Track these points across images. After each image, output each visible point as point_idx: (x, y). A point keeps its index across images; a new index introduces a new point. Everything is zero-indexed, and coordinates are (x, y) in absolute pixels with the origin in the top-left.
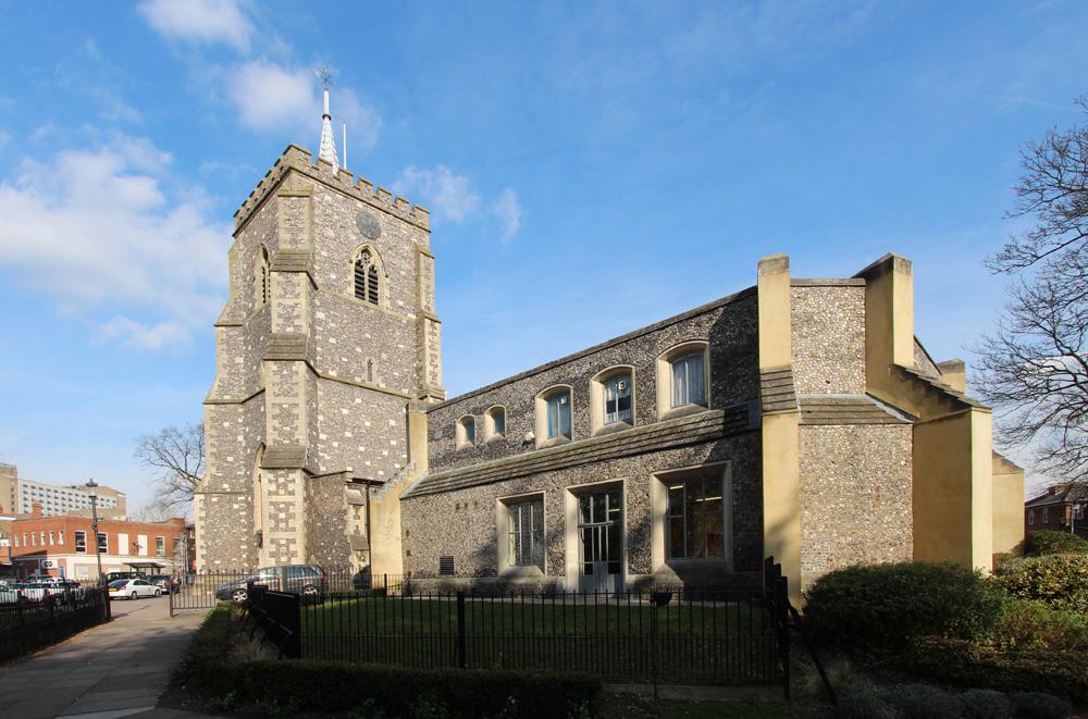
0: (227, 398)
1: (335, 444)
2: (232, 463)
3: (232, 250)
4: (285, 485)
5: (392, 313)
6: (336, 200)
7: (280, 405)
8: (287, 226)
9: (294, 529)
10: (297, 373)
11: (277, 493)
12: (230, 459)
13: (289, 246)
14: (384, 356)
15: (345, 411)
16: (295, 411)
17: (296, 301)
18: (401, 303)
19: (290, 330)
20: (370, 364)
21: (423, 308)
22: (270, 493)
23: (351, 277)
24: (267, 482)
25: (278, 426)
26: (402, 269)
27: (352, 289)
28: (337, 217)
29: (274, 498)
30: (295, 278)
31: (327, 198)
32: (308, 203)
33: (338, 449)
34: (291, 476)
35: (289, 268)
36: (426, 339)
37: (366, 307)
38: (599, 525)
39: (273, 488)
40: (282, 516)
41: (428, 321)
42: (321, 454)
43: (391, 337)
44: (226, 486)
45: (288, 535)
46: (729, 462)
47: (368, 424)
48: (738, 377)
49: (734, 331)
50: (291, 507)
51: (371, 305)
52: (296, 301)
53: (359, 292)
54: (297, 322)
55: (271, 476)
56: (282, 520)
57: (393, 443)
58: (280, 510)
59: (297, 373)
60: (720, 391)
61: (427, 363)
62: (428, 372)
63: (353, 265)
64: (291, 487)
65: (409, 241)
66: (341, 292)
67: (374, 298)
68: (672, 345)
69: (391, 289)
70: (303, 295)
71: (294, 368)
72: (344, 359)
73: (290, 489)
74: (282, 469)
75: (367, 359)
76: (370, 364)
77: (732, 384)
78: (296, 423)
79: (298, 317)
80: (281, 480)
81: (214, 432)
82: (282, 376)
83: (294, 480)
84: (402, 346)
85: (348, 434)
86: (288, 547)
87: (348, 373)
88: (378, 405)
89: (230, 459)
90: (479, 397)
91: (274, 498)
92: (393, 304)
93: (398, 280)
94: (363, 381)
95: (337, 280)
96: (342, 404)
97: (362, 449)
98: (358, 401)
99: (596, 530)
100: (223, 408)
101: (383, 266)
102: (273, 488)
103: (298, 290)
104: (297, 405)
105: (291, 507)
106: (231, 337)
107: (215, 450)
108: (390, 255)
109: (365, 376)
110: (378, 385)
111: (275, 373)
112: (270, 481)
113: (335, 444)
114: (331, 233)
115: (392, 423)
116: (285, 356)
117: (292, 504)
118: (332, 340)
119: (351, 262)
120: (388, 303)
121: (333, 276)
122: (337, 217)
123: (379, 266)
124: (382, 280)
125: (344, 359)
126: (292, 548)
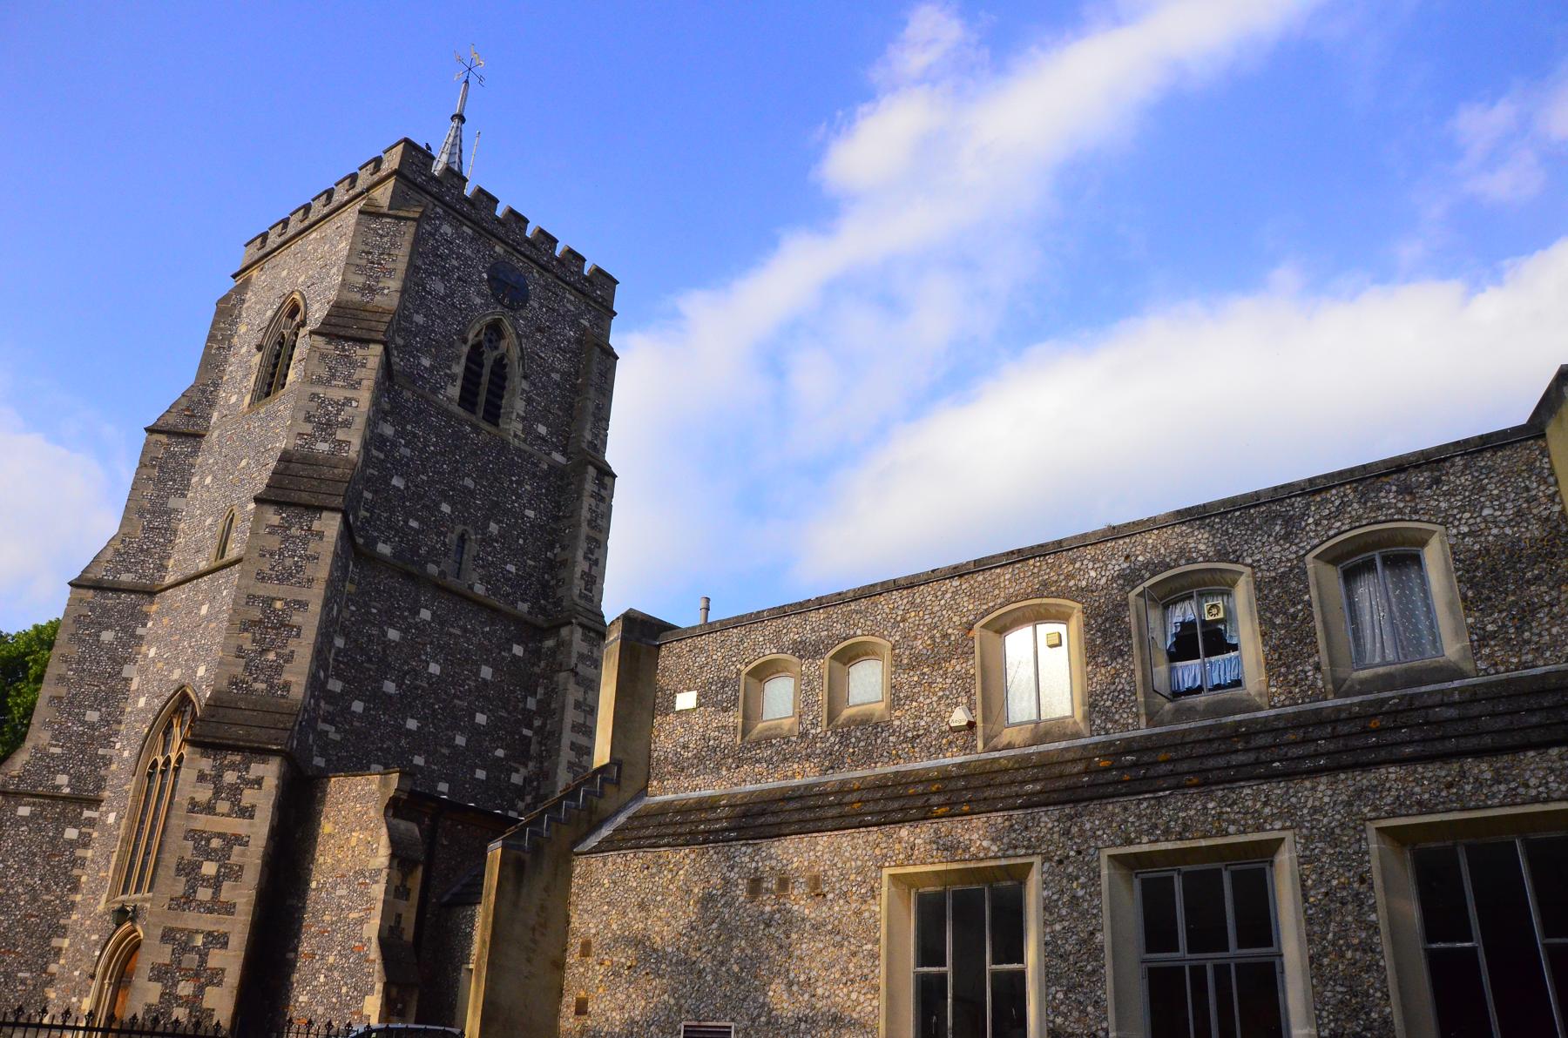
0: (126, 578)
1: (358, 706)
2: (92, 726)
3: (226, 299)
4: (235, 790)
5: (524, 447)
6: (461, 236)
7: (269, 601)
8: (364, 262)
9: (229, 909)
10: (320, 535)
11: (209, 809)
12: (92, 716)
13: (357, 297)
14: (493, 528)
15: (393, 634)
16: (297, 619)
17: (349, 393)
18: (542, 430)
19: (323, 447)
20: (462, 539)
21: (584, 445)
22: (194, 807)
23: (458, 369)
24: (194, 775)
25: (248, 646)
26: (554, 370)
27: (454, 391)
28: (455, 263)
29: (201, 822)
30: (359, 352)
31: (447, 229)
32: (412, 230)
33: (360, 717)
34: (256, 769)
35: (350, 333)
36: (585, 506)
37: (476, 429)
38: (1209, 960)
39: (204, 794)
40: (209, 869)
41: (591, 471)
42: (322, 726)
43: (514, 492)
44: (62, 779)
45: (207, 922)
46: (1037, 860)
47: (434, 669)
48: (1533, 609)
49: (1502, 508)
50: (237, 849)
51: (484, 425)
52: (349, 393)
53: (467, 400)
54: (341, 435)
55: (206, 764)
56: (206, 880)
57: (481, 719)
58: (209, 855)
59: (320, 535)
60: (1493, 635)
61: (580, 554)
62: (578, 571)
63: (465, 349)
64: (248, 796)
65: (574, 323)
66: (435, 391)
67: (493, 414)
68: (1344, 531)
69: (529, 401)
70: (368, 384)
71: (316, 525)
72: (414, 524)
73: (245, 802)
74: (236, 749)
75: (459, 528)
76: (462, 539)
77: (1525, 616)
78: (292, 644)
79: (347, 424)
80: (230, 777)
81: (75, 651)
82: (286, 539)
83: (259, 782)
84: (530, 513)
85: (390, 687)
86: (203, 956)
87: (415, 550)
88: (465, 630)
89: (92, 716)
90: (813, 616)
91: (201, 822)
92: (528, 430)
93: (544, 387)
94: (442, 573)
95: (430, 370)
96: (389, 618)
97: (412, 724)
98: (425, 614)
99: (1198, 972)
100: (110, 600)
101: (522, 358)
102: (204, 794)
103: (359, 374)
104: (303, 605)
105: (237, 849)
106: (174, 454)
107: (63, 691)
108: (536, 342)
109: (448, 564)
110: (471, 587)
111: (273, 530)
112: (202, 777)
113: (358, 706)
114: (439, 287)
115: (486, 672)
116: (305, 497)
117: (238, 840)
118: (397, 482)
119: (465, 341)
120: (517, 427)
121: (426, 362)
122: (455, 263)
123: (515, 353)
124: (518, 383)
125: (414, 524)
126: (216, 959)
